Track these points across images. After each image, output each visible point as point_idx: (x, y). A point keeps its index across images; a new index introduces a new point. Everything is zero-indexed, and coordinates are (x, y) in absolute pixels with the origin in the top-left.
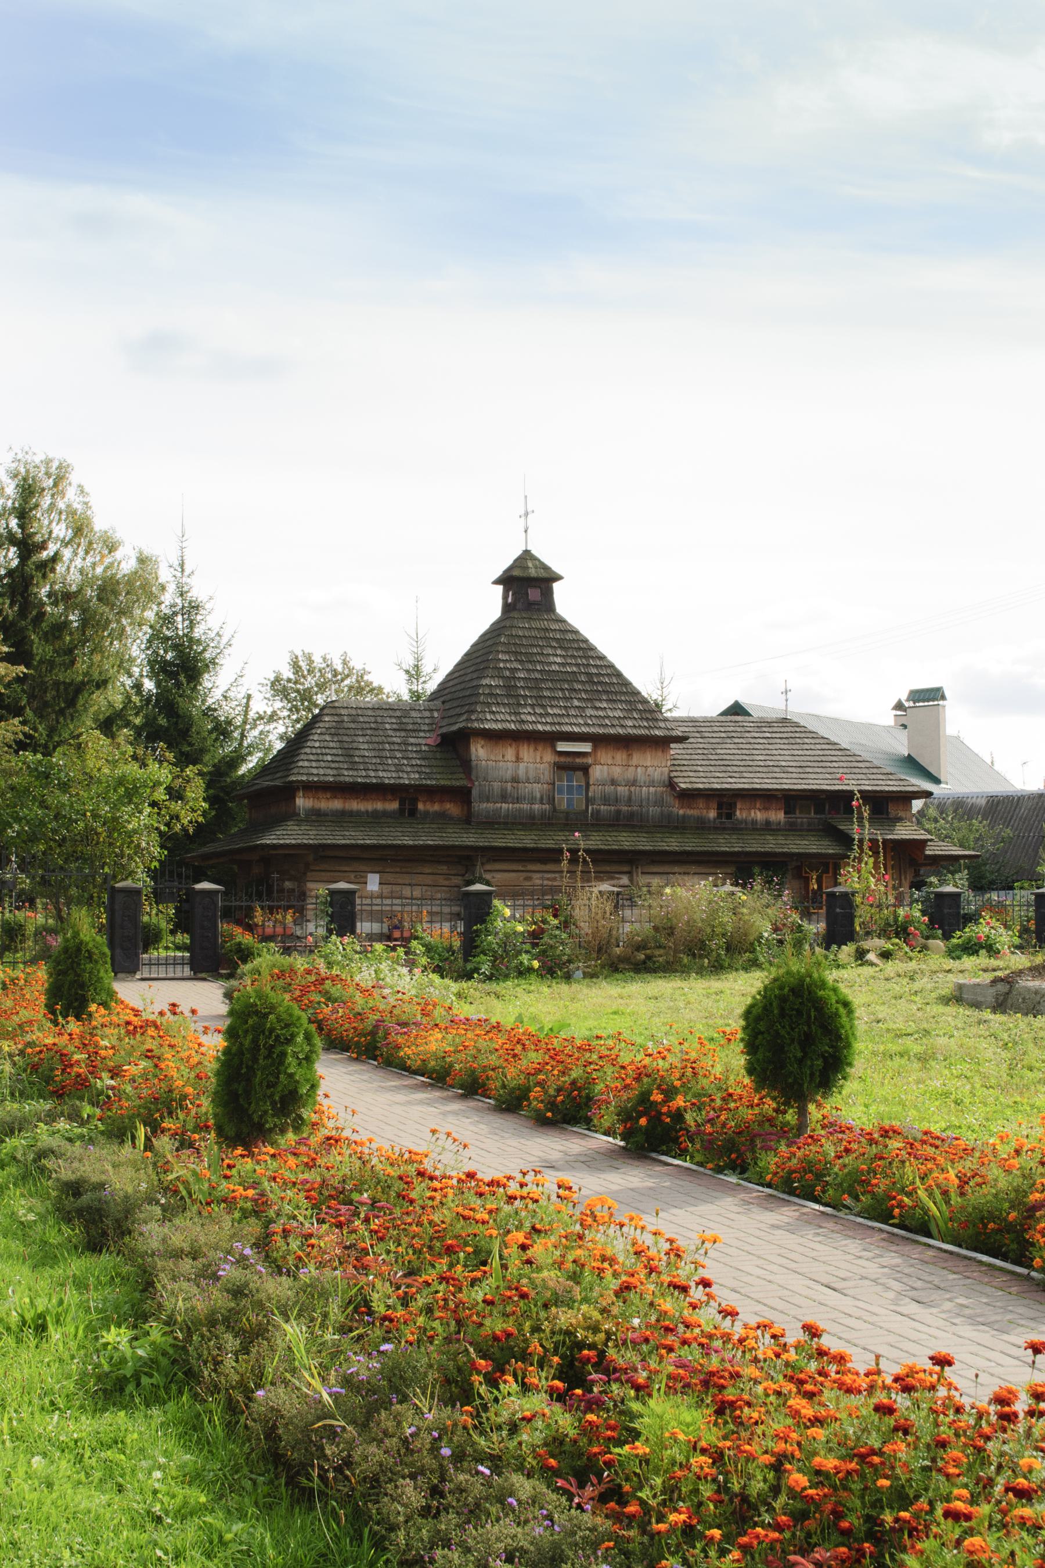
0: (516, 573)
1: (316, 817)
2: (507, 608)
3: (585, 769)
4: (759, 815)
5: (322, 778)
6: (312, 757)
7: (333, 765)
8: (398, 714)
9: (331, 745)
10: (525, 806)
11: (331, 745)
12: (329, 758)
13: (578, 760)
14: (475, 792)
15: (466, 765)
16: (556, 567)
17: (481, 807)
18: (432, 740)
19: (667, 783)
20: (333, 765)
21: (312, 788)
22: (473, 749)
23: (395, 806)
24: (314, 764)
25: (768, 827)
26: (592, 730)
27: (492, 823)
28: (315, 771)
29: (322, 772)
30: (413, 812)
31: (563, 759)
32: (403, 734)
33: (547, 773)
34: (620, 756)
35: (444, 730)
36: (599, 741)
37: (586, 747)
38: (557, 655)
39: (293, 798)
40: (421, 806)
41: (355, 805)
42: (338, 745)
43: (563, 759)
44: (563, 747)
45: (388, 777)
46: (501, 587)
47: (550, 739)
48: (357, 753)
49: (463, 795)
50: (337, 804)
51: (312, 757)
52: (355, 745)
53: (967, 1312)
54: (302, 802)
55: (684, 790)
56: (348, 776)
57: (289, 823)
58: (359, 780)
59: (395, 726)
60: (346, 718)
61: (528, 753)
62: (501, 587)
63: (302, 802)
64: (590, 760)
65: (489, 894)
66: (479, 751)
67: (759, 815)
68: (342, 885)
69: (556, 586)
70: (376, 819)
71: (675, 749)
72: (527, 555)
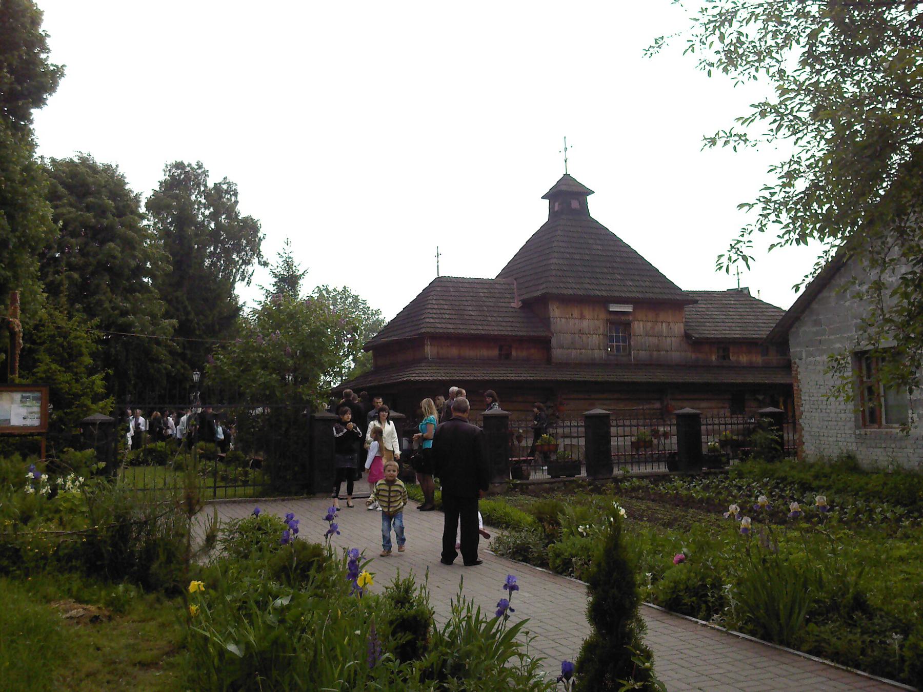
0: (564, 188)
1: (441, 361)
2: (552, 214)
3: (628, 325)
4: (744, 359)
5: (445, 331)
6: (435, 316)
7: (450, 321)
8: (487, 286)
9: (446, 307)
10: (589, 352)
11: (446, 307)
12: (447, 316)
13: (623, 318)
14: (554, 342)
15: (546, 322)
16: (588, 183)
17: (557, 353)
18: (516, 304)
19: (683, 334)
20: (450, 321)
21: (437, 338)
22: (551, 308)
23: (495, 353)
24: (437, 321)
25: (751, 367)
26: (634, 295)
27: (564, 365)
28: (439, 326)
29: (444, 326)
30: (508, 356)
31: (612, 317)
32: (494, 300)
33: (601, 326)
34: (651, 316)
35: (526, 296)
36: (638, 303)
37: (628, 308)
38: (597, 244)
39: (423, 345)
40: (514, 353)
41: (469, 353)
42: (450, 307)
43: (612, 317)
44: (614, 308)
45: (494, 330)
46: (547, 201)
47: (602, 302)
48: (465, 313)
49: (544, 343)
50: (454, 352)
51: (435, 316)
52: (462, 307)
53: (711, 648)
54: (429, 350)
55: (697, 338)
56: (463, 330)
57: (423, 364)
58: (472, 332)
59: (486, 295)
60: (451, 289)
61: (587, 313)
62: (547, 201)
63: (429, 350)
64: (631, 318)
65: (606, 416)
66: (555, 311)
67: (744, 359)
68: (688, 410)
69: (589, 198)
70: (486, 363)
71: (688, 308)
72: (567, 176)
